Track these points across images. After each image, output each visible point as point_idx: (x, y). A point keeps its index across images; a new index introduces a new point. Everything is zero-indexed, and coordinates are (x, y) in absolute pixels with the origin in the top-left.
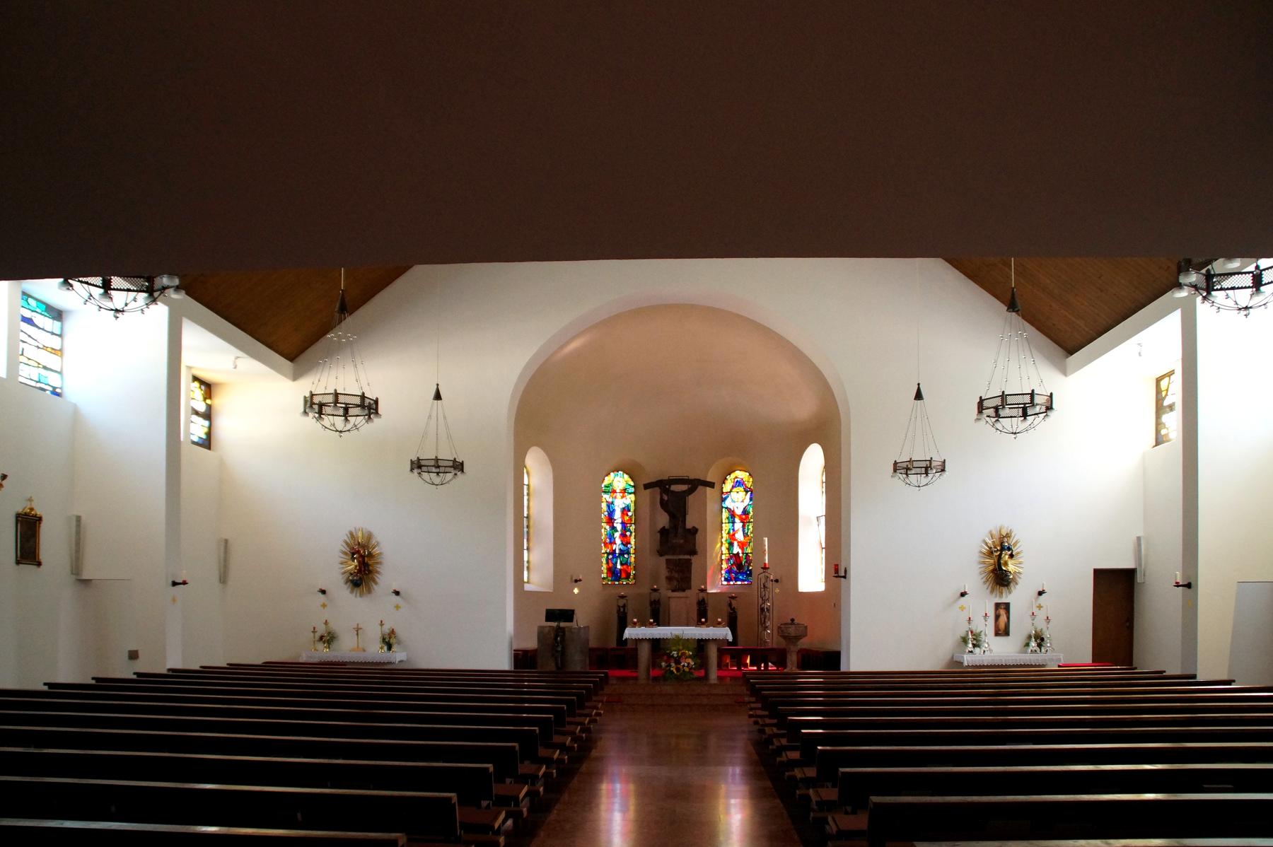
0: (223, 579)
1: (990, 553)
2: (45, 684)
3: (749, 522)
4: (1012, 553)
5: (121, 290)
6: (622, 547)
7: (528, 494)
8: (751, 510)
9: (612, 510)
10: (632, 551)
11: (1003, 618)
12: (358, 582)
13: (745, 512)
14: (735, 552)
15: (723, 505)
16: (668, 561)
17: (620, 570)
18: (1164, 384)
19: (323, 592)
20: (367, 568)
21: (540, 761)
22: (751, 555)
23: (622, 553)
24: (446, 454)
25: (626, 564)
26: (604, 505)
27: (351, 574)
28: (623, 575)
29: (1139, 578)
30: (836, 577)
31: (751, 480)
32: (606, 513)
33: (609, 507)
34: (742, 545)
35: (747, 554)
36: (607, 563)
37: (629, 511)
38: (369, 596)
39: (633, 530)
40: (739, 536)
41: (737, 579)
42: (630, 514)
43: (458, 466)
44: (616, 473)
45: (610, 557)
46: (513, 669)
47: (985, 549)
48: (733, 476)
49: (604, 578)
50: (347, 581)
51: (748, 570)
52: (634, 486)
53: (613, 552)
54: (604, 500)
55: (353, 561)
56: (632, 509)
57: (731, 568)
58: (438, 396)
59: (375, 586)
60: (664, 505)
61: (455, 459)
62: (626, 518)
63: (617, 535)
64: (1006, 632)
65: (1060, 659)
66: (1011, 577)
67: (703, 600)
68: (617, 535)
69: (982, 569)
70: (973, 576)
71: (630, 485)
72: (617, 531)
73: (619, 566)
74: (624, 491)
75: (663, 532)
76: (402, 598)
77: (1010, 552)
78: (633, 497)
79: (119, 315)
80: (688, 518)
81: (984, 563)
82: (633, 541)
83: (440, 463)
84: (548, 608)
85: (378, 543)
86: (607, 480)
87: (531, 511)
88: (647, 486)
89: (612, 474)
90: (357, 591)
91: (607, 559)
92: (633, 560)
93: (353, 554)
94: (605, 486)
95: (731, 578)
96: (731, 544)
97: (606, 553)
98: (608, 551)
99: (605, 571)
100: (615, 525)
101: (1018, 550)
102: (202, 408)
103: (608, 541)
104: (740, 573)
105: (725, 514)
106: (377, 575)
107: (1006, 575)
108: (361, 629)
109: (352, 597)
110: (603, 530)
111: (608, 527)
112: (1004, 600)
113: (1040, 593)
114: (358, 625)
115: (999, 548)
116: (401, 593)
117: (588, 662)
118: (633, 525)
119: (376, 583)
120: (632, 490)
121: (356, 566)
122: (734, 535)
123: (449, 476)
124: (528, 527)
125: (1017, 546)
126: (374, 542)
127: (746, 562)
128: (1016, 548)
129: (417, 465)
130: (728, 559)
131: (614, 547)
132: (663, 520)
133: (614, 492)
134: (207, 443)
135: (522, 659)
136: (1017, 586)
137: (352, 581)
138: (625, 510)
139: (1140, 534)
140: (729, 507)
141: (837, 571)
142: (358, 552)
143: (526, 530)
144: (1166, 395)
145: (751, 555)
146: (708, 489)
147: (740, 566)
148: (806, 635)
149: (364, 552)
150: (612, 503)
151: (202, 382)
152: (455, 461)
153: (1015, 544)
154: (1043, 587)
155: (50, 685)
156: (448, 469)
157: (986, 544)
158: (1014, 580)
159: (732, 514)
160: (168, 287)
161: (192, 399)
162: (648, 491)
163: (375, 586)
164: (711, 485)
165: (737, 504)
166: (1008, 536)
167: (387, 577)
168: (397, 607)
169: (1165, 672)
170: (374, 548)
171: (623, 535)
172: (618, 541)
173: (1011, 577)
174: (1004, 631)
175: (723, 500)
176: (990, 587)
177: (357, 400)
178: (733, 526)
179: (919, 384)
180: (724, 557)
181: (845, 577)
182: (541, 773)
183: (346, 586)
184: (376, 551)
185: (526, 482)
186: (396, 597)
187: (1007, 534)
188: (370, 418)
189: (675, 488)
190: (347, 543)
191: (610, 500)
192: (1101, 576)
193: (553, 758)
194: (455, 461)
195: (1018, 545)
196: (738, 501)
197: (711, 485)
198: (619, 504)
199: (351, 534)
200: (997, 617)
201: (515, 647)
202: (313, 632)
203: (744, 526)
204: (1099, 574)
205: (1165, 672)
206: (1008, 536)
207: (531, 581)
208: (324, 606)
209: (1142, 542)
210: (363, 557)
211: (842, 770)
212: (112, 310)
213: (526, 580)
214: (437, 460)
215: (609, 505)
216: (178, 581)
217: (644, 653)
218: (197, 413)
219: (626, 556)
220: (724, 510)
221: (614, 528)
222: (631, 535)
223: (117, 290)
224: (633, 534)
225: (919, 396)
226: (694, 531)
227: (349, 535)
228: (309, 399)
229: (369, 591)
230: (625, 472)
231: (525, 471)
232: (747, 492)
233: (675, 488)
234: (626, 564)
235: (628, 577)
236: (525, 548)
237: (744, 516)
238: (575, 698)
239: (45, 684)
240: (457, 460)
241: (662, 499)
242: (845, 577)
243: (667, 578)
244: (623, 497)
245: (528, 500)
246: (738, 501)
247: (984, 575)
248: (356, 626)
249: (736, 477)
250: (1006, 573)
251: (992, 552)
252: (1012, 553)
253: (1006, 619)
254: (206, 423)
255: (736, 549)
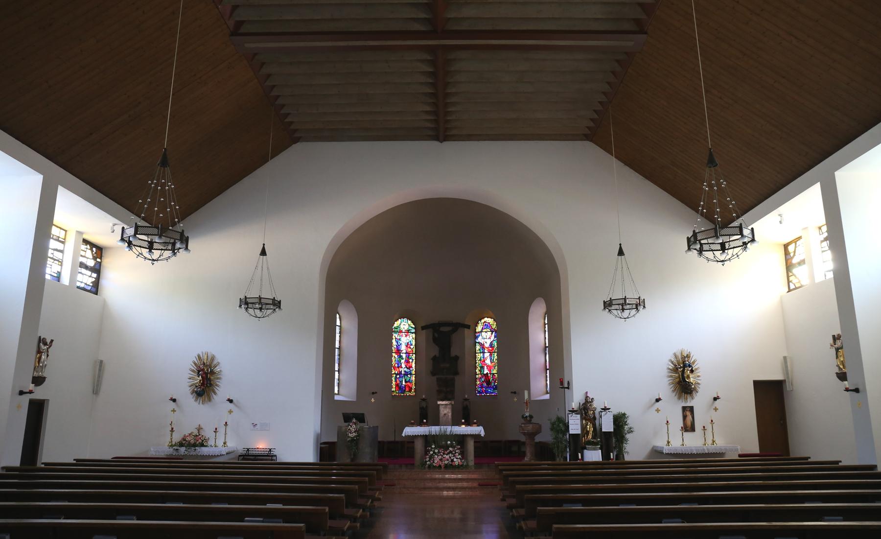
0: (96, 391)
1: (675, 370)
2: (74, 460)
3: (494, 352)
4: (692, 369)
5: (158, 249)
6: (406, 370)
7: (340, 333)
8: (496, 344)
9: (399, 344)
10: (413, 372)
11: (689, 418)
12: (201, 393)
13: (491, 345)
14: (485, 373)
15: (477, 341)
16: (438, 380)
17: (405, 386)
18: (791, 248)
19: (174, 400)
20: (209, 382)
21: (359, 506)
22: (496, 375)
23: (406, 374)
24: (267, 294)
25: (409, 381)
26: (394, 341)
27: (196, 386)
28: (407, 390)
29: (788, 387)
30: (562, 388)
31: (495, 323)
32: (395, 346)
33: (397, 342)
34: (489, 368)
35: (493, 374)
36: (396, 381)
37: (412, 345)
38: (208, 402)
39: (414, 358)
40: (488, 362)
41: (486, 392)
42: (412, 347)
43: (277, 304)
44: (402, 319)
45: (398, 376)
46: (319, 462)
47: (671, 366)
48: (483, 321)
49: (393, 391)
50: (193, 392)
51: (494, 385)
52: (415, 328)
53: (400, 373)
54: (394, 337)
55: (199, 377)
56: (414, 344)
57: (482, 384)
58: (263, 253)
59: (214, 395)
60: (435, 340)
61: (274, 298)
62: (409, 350)
63: (403, 361)
64: (692, 429)
65: (738, 449)
66: (693, 387)
67: (467, 406)
68: (403, 361)
69: (670, 381)
70: (663, 386)
71: (412, 327)
72: (403, 359)
73: (404, 383)
74: (408, 331)
75: (434, 359)
76: (234, 404)
77: (690, 369)
78: (414, 335)
79: (155, 262)
80: (452, 349)
81: (671, 376)
82: (414, 365)
83: (263, 301)
84: (50, 402)
85: (219, 363)
86: (396, 324)
87: (342, 345)
88: (423, 328)
89: (400, 320)
90: (200, 399)
91: (396, 378)
92: (414, 379)
93: (199, 371)
94: (395, 328)
95: (482, 391)
96: (482, 367)
97: (395, 374)
98: (396, 372)
99: (394, 387)
100: (401, 354)
101: (696, 367)
102: (91, 263)
103: (396, 365)
104: (489, 387)
105: (478, 347)
106: (217, 387)
107: (689, 386)
108: (202, 428)
109: (196, 404)
110: (393, 358)
111: (396, 356)
112: (688, 404)
113: (715, 399)
114: (199, 425)
115: (682, 366)
116: (234, 401)
117: (376, 454)
118: (414, 355)
119: (215, 393)
120: (413, 331)
121: (200, 381)
122: (484, 361)
123: (269, 311)
124: (339, 355)
125: (695, 364)
126: (215, 362)
127: (493, 380)
128: (694, 365)
129: (245, 303)
130: (480, 378)
131: (401, 369)
132: (435, 351)
133: (401, 332)
134: (94, 290)
135: (326, 450)
136: (698, 394)
137: (196, 392)
138: (408, 345)
139: (786, 355)
140: (480, 342)
141: (562, 382)
142: (203, 370)
143: (337, 357)
144: (794, 255)
145: (496, 375)
146: (466, 330)
147: (488, 382)
148: (541, 432)
149: (208, 370)
150: (400, 339)
151: (92, 245)
152: (274, 299)
153: (694, 362)
154: (717, 393)
155: (77, 460)
156: (268, 306)
157: (672, 362)
158: (695, 389)
159: (482, 346)
160: (180, 248)
161: (81, 256)
162: (425, 331)
163: (214, 395)
164: (468, 327)
165: (485, 340)
166: (688, 356)
167: (223, 390)
168: (230, 412)
169: (810, 458)
170: (215, 368)
171: (407, 362)
172: (403, 366)
173: (693, 387)
174: (690, 428)
175: (477, 337)
176: (678, 394)
177: (271, 302)
178: (483, 355)
179: (620, 244)
180: (477, 376)
181: (568, 388)
182: (359, 515)
183: (192, 396)
184: (217, 369)
185: (338, 323)
186: (230, 404)
187: (687, 355)
188: (275, 310)
189: (443, 329)
190: (195, 364)
191: (399, 337)
192: (761, 387)
193: (357, 516)
194: (274, 299)
195: (696, 363)
196: (486, 338)
197: (468, 327)
198: (404, 340)
199: (199, 356)
200: (685, 417)
201: (324, 440)
202: (214, 432)
203: (491, 355)
204: (758, 385)
205: (810, 458)
206: (688, 356)
207: (340, 393)
208: (174, 411)
209: (788, 360)
210: (206, 374)
211: (539, 508)
212: (150, 260)
213: (336, 391)
214: (260, 298)
215: (398, 340)
216: (25, 391)
217: (419, 446)
218: (86, 267)
219: (409, 376)
220: (477, 344)
221: (400, 357)
222: (412, 361)
223: (156, 249)
224: (414, 361)
225: (621, 253)
226: (456, 358)
227: (197, 358)
228: (244, 300)
229: (210, 400)
230: (409, 318)
231: (338, 316)
232: (492, 332)
233: (443, 329)
234: (409, 381)
235: (410, 390)
236: (336, 369)
237: (491, 349)
238: (381, 467)
239: (74, 460)
240: (276, 299)
241: (434, 335)
242: (568, 388)
243: (437, 391)
244: (406, 336)
245: (340, 336)
246: (486, 338)
247: (672, 386)
248: (198, 427)
249: (485, 322)
250: (689, 384)
251: (677, 369)
252: (692, 369)
253: (691, 419)
254: (95, 275)
255: (486, 371)
